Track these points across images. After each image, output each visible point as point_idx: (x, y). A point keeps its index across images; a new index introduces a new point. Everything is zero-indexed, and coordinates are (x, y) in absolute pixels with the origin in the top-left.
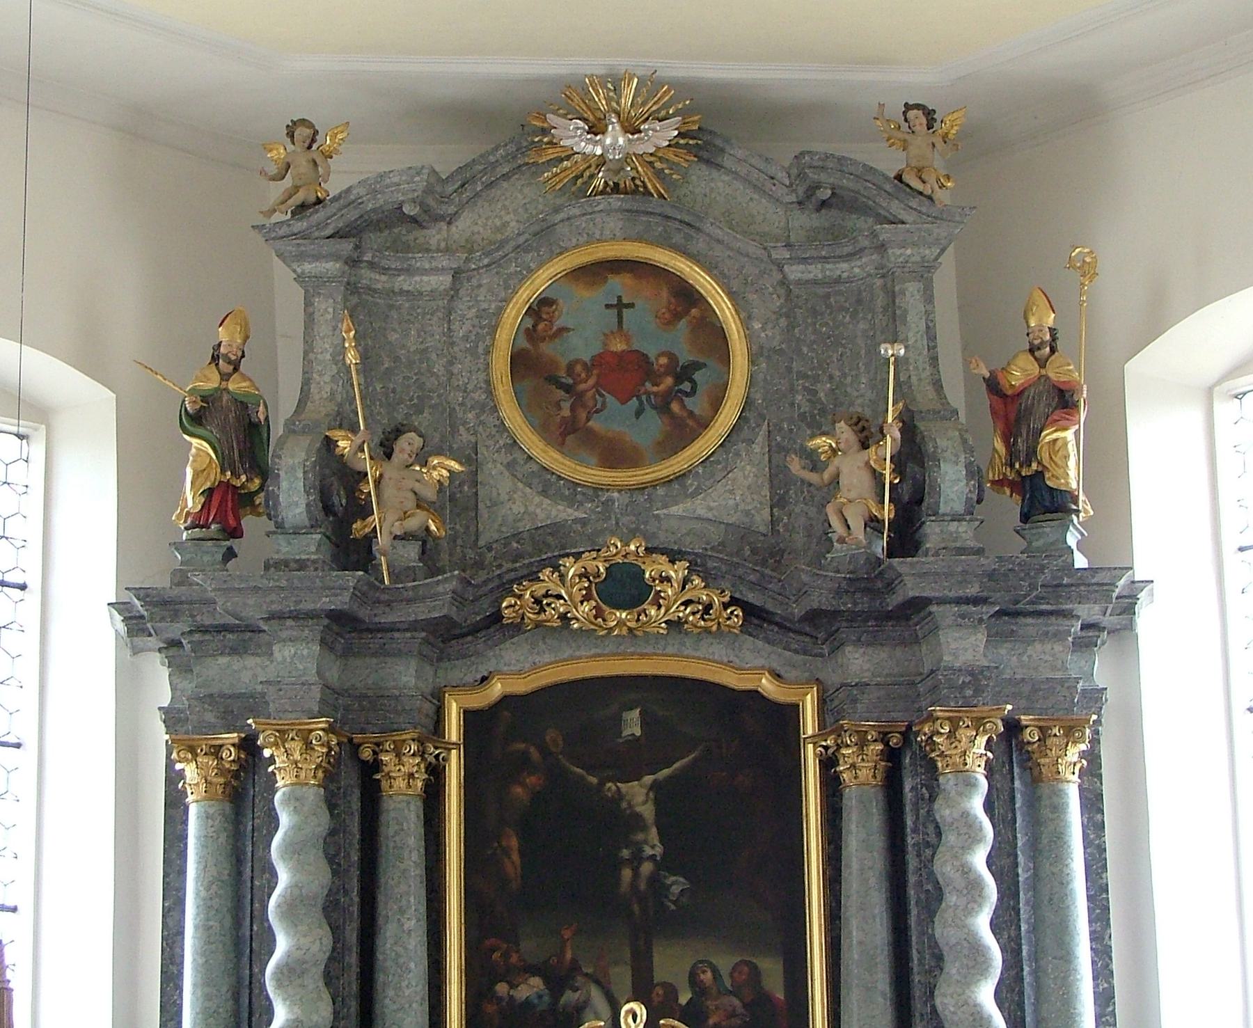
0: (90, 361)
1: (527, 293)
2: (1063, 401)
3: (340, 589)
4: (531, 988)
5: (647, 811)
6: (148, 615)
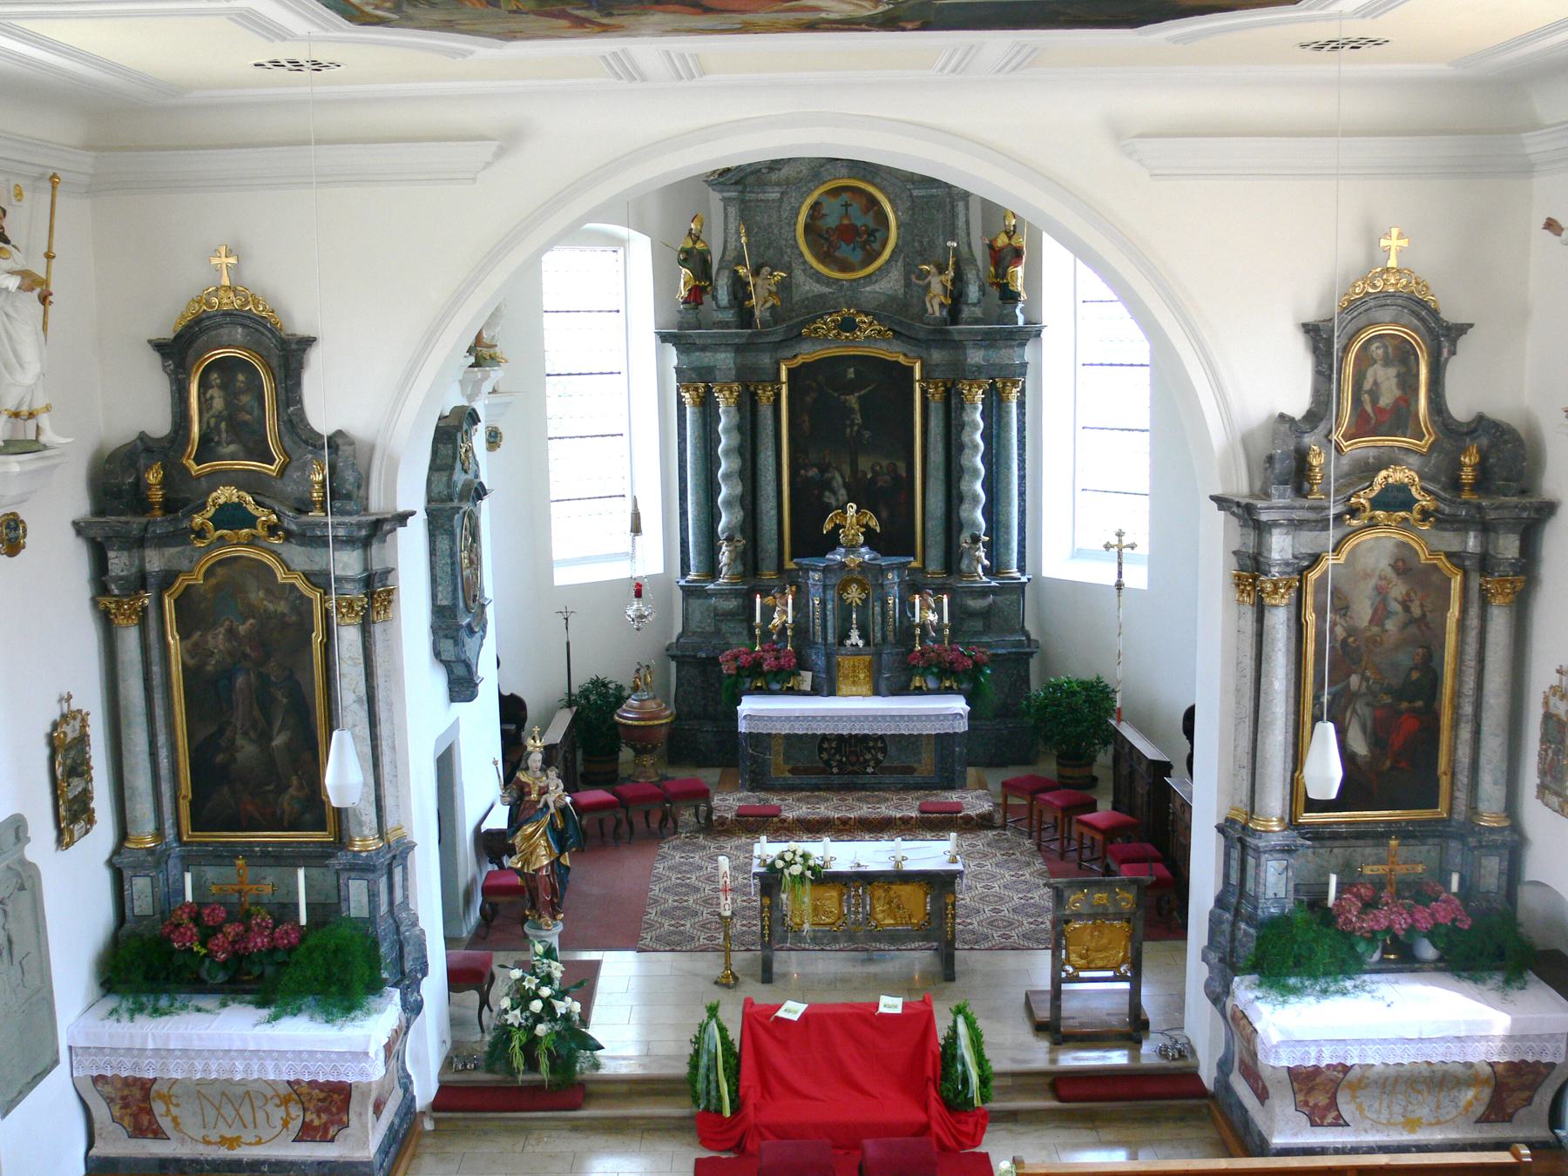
1: (809, 202)
4: (813, 472)
5: (856, 406)
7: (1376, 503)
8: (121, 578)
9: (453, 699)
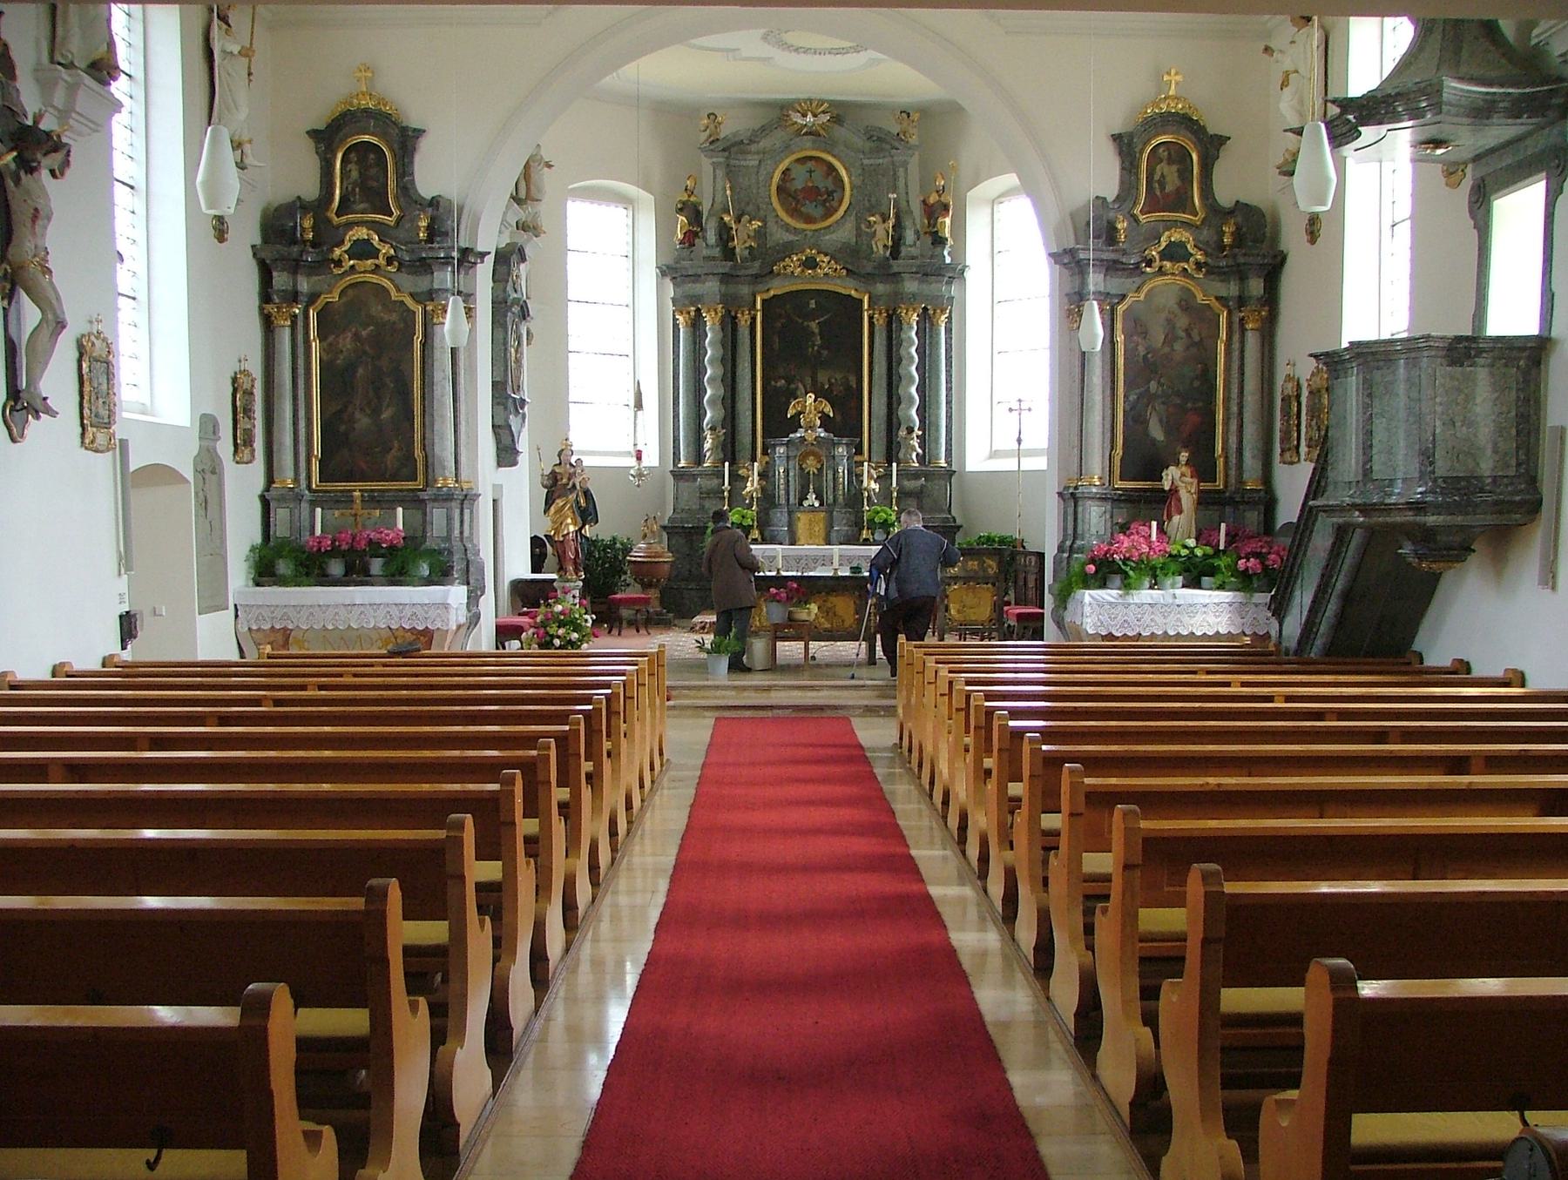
1: (782, 167)
3: (726, 267)
6: (665, 271)
7: (1164, 255)
9: (499, 464)
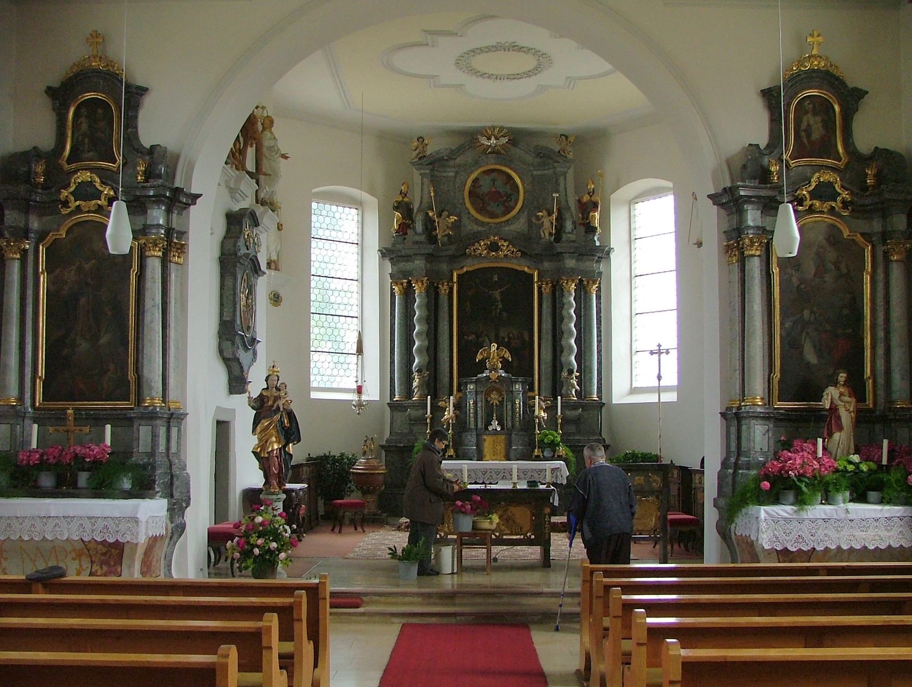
0: (372, 193)
2: (595, 206)
3: (430, 249)
5: (499, 298)
6: (385, 253)
7: (814, 195)
8: (11, 227)
